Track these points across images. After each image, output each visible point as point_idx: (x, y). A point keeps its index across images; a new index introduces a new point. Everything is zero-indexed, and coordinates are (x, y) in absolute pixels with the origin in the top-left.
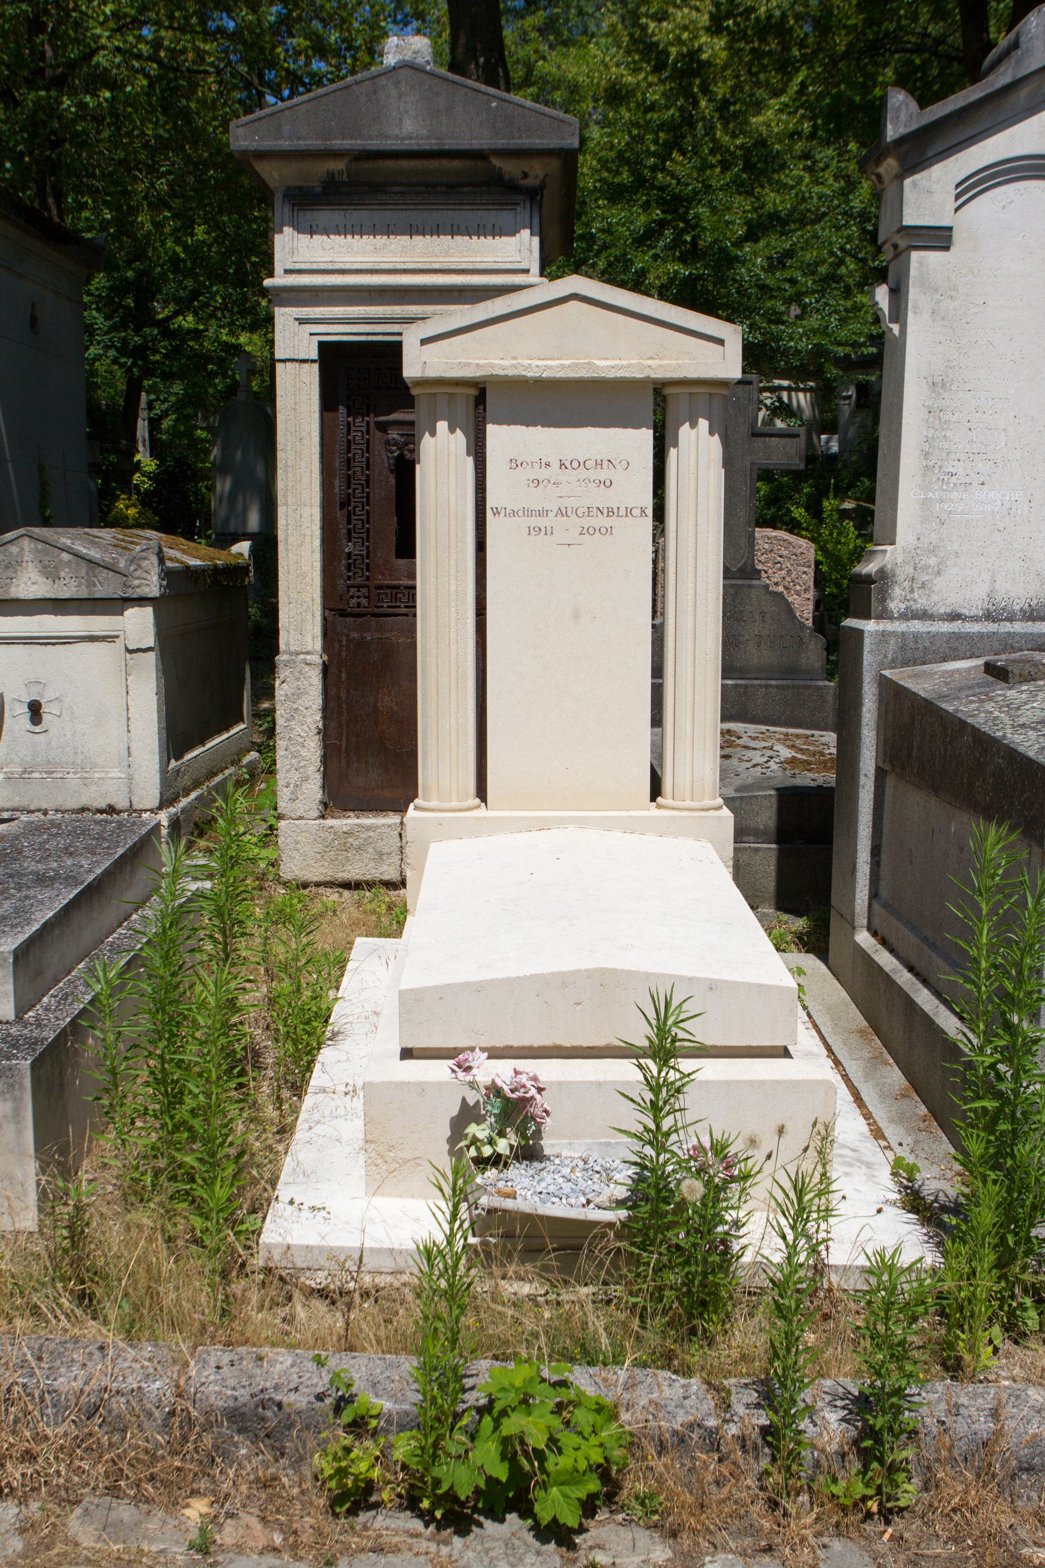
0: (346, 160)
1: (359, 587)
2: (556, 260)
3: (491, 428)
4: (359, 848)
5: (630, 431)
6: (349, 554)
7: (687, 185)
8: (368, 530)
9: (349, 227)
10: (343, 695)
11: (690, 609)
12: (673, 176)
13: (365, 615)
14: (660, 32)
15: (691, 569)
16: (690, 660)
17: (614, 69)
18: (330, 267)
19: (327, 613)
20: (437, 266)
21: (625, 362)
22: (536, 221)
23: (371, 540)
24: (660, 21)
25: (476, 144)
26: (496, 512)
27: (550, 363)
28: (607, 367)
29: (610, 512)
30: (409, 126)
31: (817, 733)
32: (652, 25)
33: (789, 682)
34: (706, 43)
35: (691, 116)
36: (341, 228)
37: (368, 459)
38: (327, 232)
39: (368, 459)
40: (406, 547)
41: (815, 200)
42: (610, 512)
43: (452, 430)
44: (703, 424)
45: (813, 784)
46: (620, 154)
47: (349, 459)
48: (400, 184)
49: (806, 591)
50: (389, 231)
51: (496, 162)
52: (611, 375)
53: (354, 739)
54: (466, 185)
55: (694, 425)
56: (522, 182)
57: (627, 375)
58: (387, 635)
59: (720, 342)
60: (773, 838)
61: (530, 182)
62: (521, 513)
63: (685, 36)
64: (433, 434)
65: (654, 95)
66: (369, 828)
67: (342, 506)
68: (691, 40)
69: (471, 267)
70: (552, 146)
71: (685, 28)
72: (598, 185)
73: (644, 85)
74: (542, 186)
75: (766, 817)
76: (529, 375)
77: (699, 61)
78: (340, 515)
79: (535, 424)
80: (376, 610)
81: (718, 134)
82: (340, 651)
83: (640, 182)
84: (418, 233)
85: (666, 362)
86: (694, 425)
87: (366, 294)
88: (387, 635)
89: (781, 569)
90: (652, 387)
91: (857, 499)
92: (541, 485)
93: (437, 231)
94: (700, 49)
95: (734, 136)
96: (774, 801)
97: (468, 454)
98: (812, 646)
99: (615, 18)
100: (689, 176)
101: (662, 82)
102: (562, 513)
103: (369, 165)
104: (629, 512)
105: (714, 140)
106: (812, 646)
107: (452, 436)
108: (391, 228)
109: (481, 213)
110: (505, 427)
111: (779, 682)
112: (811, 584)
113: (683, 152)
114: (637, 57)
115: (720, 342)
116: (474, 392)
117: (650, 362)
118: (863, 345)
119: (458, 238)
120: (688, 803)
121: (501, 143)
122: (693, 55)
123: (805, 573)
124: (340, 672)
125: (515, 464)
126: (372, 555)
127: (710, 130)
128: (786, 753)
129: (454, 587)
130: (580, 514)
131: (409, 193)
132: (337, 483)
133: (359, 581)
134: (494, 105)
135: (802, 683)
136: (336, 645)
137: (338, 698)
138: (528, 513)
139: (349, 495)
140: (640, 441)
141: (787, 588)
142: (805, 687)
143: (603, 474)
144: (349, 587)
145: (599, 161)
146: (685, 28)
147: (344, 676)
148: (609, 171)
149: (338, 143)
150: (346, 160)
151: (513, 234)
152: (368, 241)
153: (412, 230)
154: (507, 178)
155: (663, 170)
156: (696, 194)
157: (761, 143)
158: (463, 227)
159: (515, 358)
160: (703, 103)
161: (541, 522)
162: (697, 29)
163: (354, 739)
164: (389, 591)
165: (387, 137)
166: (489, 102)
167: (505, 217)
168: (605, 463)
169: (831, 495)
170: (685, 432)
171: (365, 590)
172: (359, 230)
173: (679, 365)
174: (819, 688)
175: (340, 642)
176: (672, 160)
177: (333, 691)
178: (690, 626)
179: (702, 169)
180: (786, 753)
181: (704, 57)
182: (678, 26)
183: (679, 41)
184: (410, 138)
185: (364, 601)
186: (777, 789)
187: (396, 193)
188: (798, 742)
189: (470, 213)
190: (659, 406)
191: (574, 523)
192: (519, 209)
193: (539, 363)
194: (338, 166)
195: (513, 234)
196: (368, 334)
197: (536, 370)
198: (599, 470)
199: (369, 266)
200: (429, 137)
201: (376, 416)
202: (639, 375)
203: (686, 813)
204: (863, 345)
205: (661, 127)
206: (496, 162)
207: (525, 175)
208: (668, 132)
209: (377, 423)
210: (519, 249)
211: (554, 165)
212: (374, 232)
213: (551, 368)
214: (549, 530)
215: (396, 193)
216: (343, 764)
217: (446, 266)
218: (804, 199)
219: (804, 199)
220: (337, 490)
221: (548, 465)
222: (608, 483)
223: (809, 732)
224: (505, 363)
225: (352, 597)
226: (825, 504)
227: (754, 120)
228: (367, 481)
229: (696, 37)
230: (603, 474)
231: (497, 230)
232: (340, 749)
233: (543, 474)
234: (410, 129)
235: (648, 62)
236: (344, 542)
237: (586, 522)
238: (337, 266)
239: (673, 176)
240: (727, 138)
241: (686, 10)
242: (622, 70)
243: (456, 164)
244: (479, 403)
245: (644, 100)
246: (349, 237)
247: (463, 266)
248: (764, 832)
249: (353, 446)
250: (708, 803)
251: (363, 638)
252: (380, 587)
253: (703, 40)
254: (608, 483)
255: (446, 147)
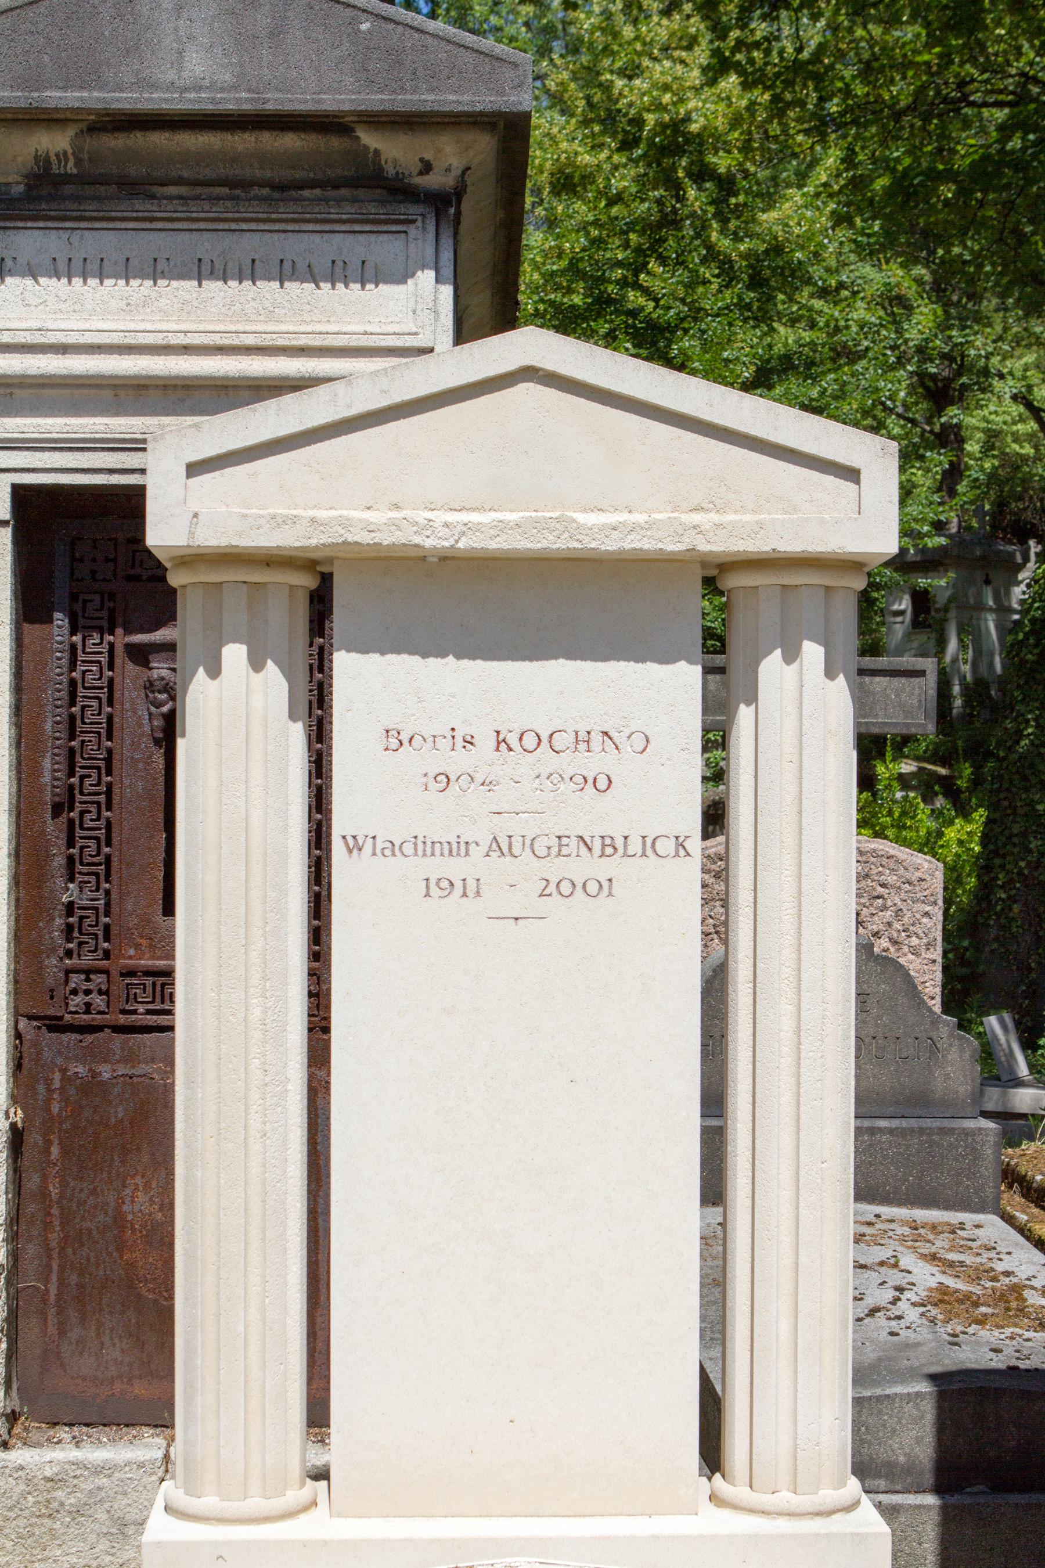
0: (71, 132)
1: (88, 972)
2: (489, 305)
3: (342, 662)
4: (77, 1512)
5: (652, 669)
6: (70, 908)
7: (669, 308)
8: (108, 859)
9: (77, 263)
10: (54, 1191)
11: (787, 1062)
12: (646, 292)
13: (99, 1028)
14: (632, 94)
15: (788, 972)
16: (786, 1175)
17: (564, 145)
18: (38, 339)
19: (23, 1023)
20: (249, 340)
21: (640, 518)
22: (447, 256)
23: (114, 877)
24: (630, 78)
25: (330, 102)
26: (354, 846)
27: (474, 517)
28: (602, 528)
29: (608, 846)
30: (197, 65)
31: (968, 1218)
32: (620, 83)
33: (913, 1123)
34: (697, 109)
35: (675, 211)
36: (62, 265)
37: (110, 718)
38: (32, 272)
39: (110, 718)
40: (169, 909)
41: (854, 329)
42: (608, 846)
43: (256, 664)
44: (813, 652)
45: (998, 1362)
46: (574, 263)
47: (72, 718)
48: (179, 181)
49: (928, 946)
50: (156, 270)
51: (369, 139)
52: (611, 544)
53: (74, 1278)
54: (311, 185)
55: (791, 655)
56: (419, 180)
57: (647, 545)
58: (142, 1069)
59: (852, 474)
60: (929, 1479)
61: (434, 181)
62: (408, 849)
63: (667, 98)
64: (214, 671)
65: (622, 182)
66: (99, 1470)
67: (57, 810)
68: (674, 104)
69: (317, 342)
70: (479, 108)
71: (666, 88)
72: (541, 307)
73: (607, 167)
74: (460, 191)
75: (916, 1439)
76: (428, 543)
77: (684, 134)
78: (53, 829)
79: (441, 653)
80: (122, 1019)
81: (714, 236)
82: (49, 1100)
83: (602, 304)
84: (212, 275)
85: (731, 517)
86: (791, 655)
87: (107, 394)
88: (142, 1069)
89: (884, 908)
90: (698, 574)
91: (917, 759)
92: (454, 787)
93: (251, 271)
94: (687, 119)
95: (737, 239)
96: (929, 1411)
97: (293, 717)
98: (953, 1055)
99: (565, 75)
100: (673, 294)
101: (635, 162)
102: (499, 847)
103: (118, 142)
104: (650, 846)
105: (710, 247)
106: (953, 1055)
107: (257, 678)
108: (161, 265)
109: (338, 238)
110: (375, 657)
111: (894, 1123)
112: (939, 935)
113: (663, 260)
114: (597, 128)
115: (852, 474)
116: (309, 582)
117: (696, 518)
118: (928, 535)
119: (291, 286)
120: (785, 1498)
121: (376, 100)
122: (677, 126)
123: (926, 914)
124: (48, 1143)
125: (396, 739)
126: (115, 909)
127: (701, 230)
128: (926, 1277)
129: (257, 1013)
130: (541, 851)
131: (197, 198)
132: (47, 763)
133: (87, 960)
134: (364, 27)
135: (936, 1123)
136: (41, 1088)
137: (43, 1194)
138: (425, 847)
139: (71, 787)
140: (677, 686)
141: (895, 942)
142: (943, 1131)
143: (594, 762)
144: (68, 972)
145: (543, 275)
146: (666, 88)
147: (55, 1151)
148: (558, 288)
149: (55, 97)
150: (71, 132)
151: (402, 278)
152: (114, 290)
153: (201, 270)
154: (390, 171)
155: (636, 286)
156: (682, 320)
157: (776, 249)
158: (302, 266)
159: (397, 507)
160: (692, 193)
161: (454, 868)
162: (683, 89)
163: (74, 1278)
164: (149, 981)
165: (154, 86)
166: (354, 23)
167: (385, 247)
168: (596, 738)
169: (889, 756)
170: (772, 668)
171: (99, 979)
172: (97, 269)
173: (761, 526)
174: (967, 1133)
175: (48, 1082)
176: (648, 273)
177: (32, 1182)
178: (787, 1098)
179: (690, 286)
180: (926, 1277)
181: (694, 127)
182: (654, 85)
183: (660, 107)
184: (199, 88)
185: (99, 1001)
186: (933, 1378)
187: (171, 198)
188: (940, 1244)
189: (316, 238)
190: (716, 614)
191: (528, 869)
192: (412, 231)
193: (451, 517)
194: (56, 142)
195: (402, 280)
196: (112, 471)
197: (443, 532)
198: (582, 755)
199: (115, 339)
200: (235, 88)
201: (128, 632)
202: (672, 547)
203: (783, 1525)
204: (928, 535)
205: (631, 227)
206: (369, 139)
207: (427, 167)
208: (642, 233)
209: (130, 648)
210: (417, 302)
211: (482, 148)
212: (127, 272)
213: (477, 528)
214: (471, 885)
215: (171, 198)
216: (52, 1330)
217: (267, 341)
218: (837, 330)
219: (837, 330)
220: (47, 779)
221: (469, 742)
222: (602, 784)
223: (954, 1217)
224: (373, 516)
225: (74, 992)
226: (880, 769)
227: (765, 217)
228: (109, 760)
229: (682, 101)
230: (592, 763)
231: (369, 272)
232: (44, 1300)
233: (458, 761)
234: (198, 71)
235: (613, 136)
236: (60, 882)
237: (556, 869)
238: (52, 338)
239: (646, 292)
240: (727, 242)
241: (667, 64)
242: (576, 146)
243: (290, 142)
244: (317, 605)
245: (608, 186)
246: (77, 281)
247: (302, 341)
248: (909, 1470)
249: (81, 692)
250: (828, 1496)
251: (94, 1074)
252: (131, 973)
253: (691, 105)
254: (602, 784)
255: (270, 106)
